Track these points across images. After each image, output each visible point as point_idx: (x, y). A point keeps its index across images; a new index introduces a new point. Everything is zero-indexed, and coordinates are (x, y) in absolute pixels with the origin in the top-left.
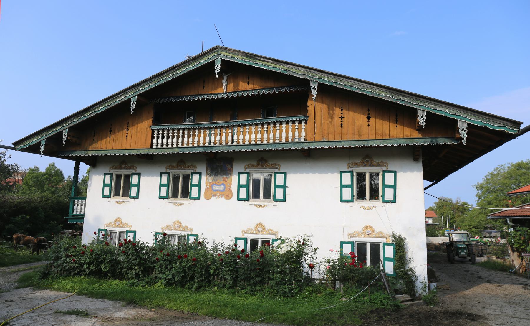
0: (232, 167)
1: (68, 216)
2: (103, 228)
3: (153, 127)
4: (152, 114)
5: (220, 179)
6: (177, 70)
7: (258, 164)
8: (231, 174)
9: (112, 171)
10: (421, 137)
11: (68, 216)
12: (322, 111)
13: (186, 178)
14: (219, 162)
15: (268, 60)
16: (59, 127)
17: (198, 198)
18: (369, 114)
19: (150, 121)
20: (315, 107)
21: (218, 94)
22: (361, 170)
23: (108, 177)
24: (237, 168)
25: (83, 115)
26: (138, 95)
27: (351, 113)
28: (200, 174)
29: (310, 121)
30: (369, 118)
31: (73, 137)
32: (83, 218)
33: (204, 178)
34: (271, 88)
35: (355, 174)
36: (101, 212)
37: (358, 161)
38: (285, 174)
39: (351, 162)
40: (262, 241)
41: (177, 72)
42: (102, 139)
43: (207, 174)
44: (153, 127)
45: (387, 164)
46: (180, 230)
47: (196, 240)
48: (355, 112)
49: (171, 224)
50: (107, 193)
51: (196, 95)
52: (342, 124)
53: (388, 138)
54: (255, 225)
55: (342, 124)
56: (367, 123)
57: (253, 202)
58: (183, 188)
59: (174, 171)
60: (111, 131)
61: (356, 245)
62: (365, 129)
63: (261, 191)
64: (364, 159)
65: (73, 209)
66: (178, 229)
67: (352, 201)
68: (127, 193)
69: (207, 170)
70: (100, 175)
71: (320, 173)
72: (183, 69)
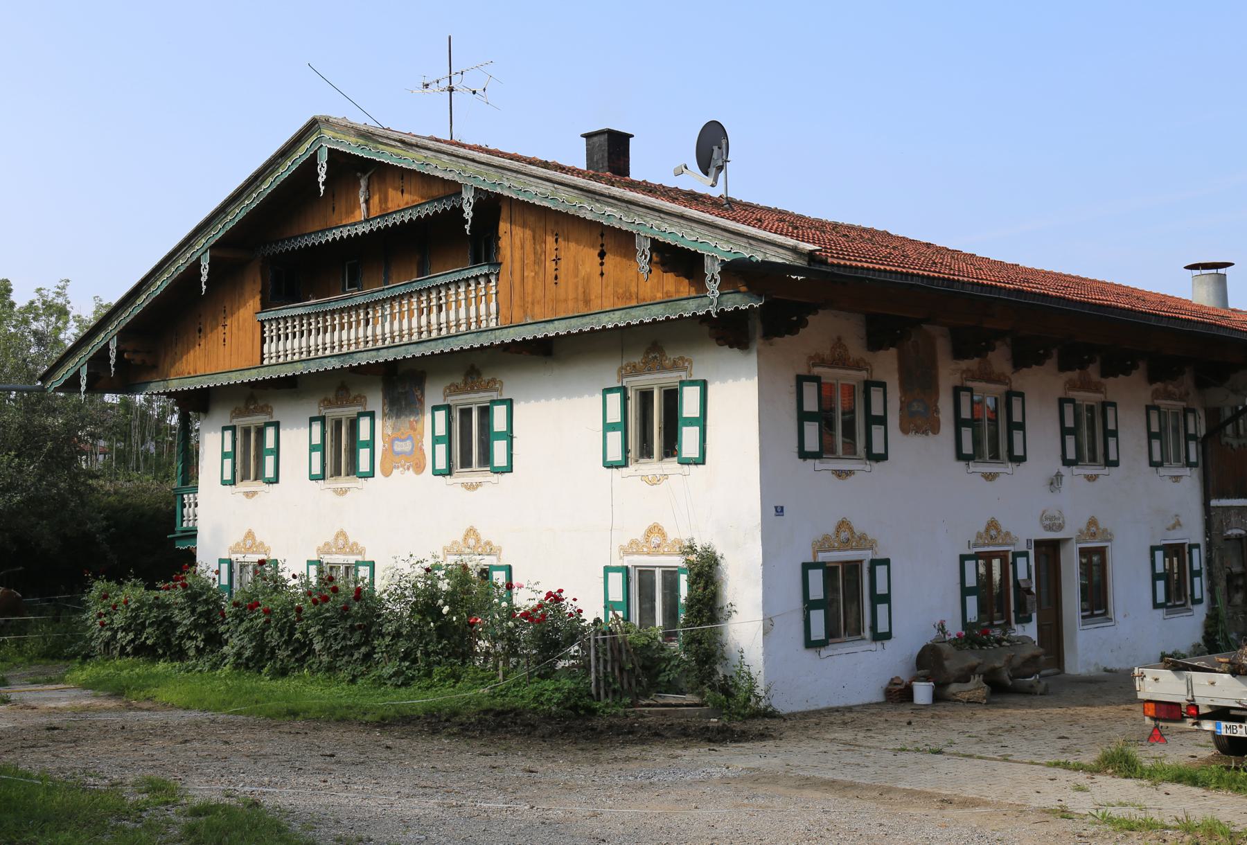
0: (423, 394)
1: (174, 532)
2: (226, 556)
3: (263, 316)
4: (259, 287)
5: (405, 422)
6: (263, 181)
7: (466, 384)
8: (421, 412)
9: (235, 422)
10: (694, 294)
11: (174, 532)
12: (522, 247)
13: (672, 398)
14: (400, 381)
15: (393, 143)
16: (102, 335)
17: (371, 474)
18: (602, 245)
19: (254, 303)
20: (512, 238)
21: (355, 224)
22: (644, 381)
23: (615, 400)
24: (434, 394)
25: (134, 302)
26: (211, 248)
27: (572, 245)
28: (372, 415)
29: (505, 269)
30: (602, 255)
31: (135, 352)
32: (195, 536)
33: (379, 423)
34: (439, 200)
35: (631, 394)
36: (266, 516)
37: (637, 359)
38: (510, 403)
39: (625, 363)
40: (663, 572)
41: (264, 187)
42: (188, 352)
43: (384, 415)
44: (263, 316)
45: (691, 363)
46: (345, 554)
47: (320, 571)
48: (578, 242)
49: (330, 538)
50: (615, 454)
51: (323, 231)
52: (556, 278)
53: (634, 304)
54: (464, 532)
55: (556, 278)
56: (554, 273)
57: (462, 477)
58: (481, 441)
59: (333, 413)
60: (200, 331)
61: (634, 577)
62: (596, 284)
63: (474, 446)
64: (647, 353)
65: (183, 516)
66: (341, 550)
67: (625, 464)
68: (671, 447)
69: (384, 404)
70: (592, 394)
71: (570, 396)
72: (271, 179)
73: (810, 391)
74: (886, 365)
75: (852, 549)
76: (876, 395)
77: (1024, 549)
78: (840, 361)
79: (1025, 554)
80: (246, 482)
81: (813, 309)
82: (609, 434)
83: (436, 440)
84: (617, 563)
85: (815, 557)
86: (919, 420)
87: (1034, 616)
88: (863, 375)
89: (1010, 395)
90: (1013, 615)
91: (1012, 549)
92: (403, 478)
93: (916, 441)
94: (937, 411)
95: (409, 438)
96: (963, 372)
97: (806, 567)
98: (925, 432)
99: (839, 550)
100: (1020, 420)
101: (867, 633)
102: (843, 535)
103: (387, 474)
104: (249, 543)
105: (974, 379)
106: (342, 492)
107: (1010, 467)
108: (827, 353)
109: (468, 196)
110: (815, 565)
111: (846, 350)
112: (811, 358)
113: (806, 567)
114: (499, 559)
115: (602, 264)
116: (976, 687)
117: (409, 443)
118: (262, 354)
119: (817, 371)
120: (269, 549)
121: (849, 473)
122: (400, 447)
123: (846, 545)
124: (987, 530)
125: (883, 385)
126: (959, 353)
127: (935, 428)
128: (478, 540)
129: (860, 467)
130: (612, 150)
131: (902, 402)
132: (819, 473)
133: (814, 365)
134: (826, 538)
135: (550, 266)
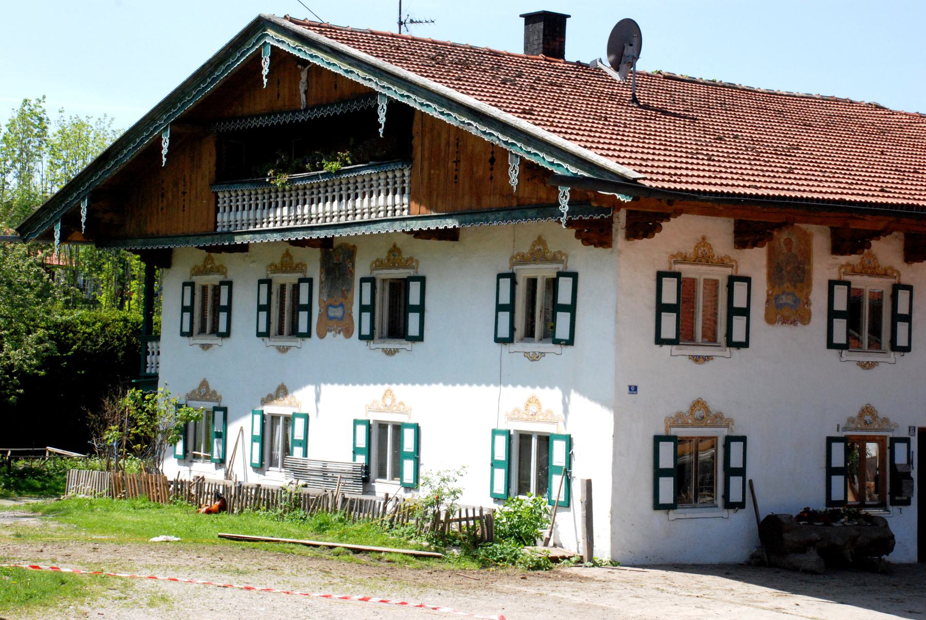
17: (308, 335)
52: (456, 177)
55: (456, 177)
69: (321, 273)
73: (670, 286)
74: (754, 262)
75: (706, 426)
76: (740, 289)
77: (905, 434)
78: (704, 257)
79: (907, 440)
80: (202, 336)
81: (667, 217)
82: (500, 314)
83: (363, 308)
84: (503, 427)
85: (667, 431)
86: (788, 309)
87: (914, 500)
88: (729, 271)
89: (896, 288)
90: (888, 497)
91: (890, 435)
92: (335, 340)
93: (781, 331)
94: (808, 303)
95: (341, 305)
96: (842, 266)
97: (658, 439)
98: (794, 323)
99: (693, 426)
100: (906, 312)
101: (720, 501)
102: (698, 414)
103: (321, 336)
104: (204, 390)
105: (854, 272)
106: (283, 350)
107: (893, 356)
108: (689, 250)
109: (383, 106)
110: (667, 438)
111: (710, 248)
112: (673, 256)
113: (658, 439)
114: (410, 417)
115: (492, 169)
116: (811, 559)
117: (340, 309)
118: (216, 222)
119: (677, 268)
120: (220, 397)
121: (707, 359)
122: (333, 312)
123: (700, 422)
124: (861, 415)
125: (747, 280)
126: (837, 249)
127: (804, 318)
128: (394, 400)
129: (718, 353)
130: (548, 30)
131: (768, 295)
132: (675, 359)
133: (676, 262)
134: (680, 415)
135: (451, 165)
